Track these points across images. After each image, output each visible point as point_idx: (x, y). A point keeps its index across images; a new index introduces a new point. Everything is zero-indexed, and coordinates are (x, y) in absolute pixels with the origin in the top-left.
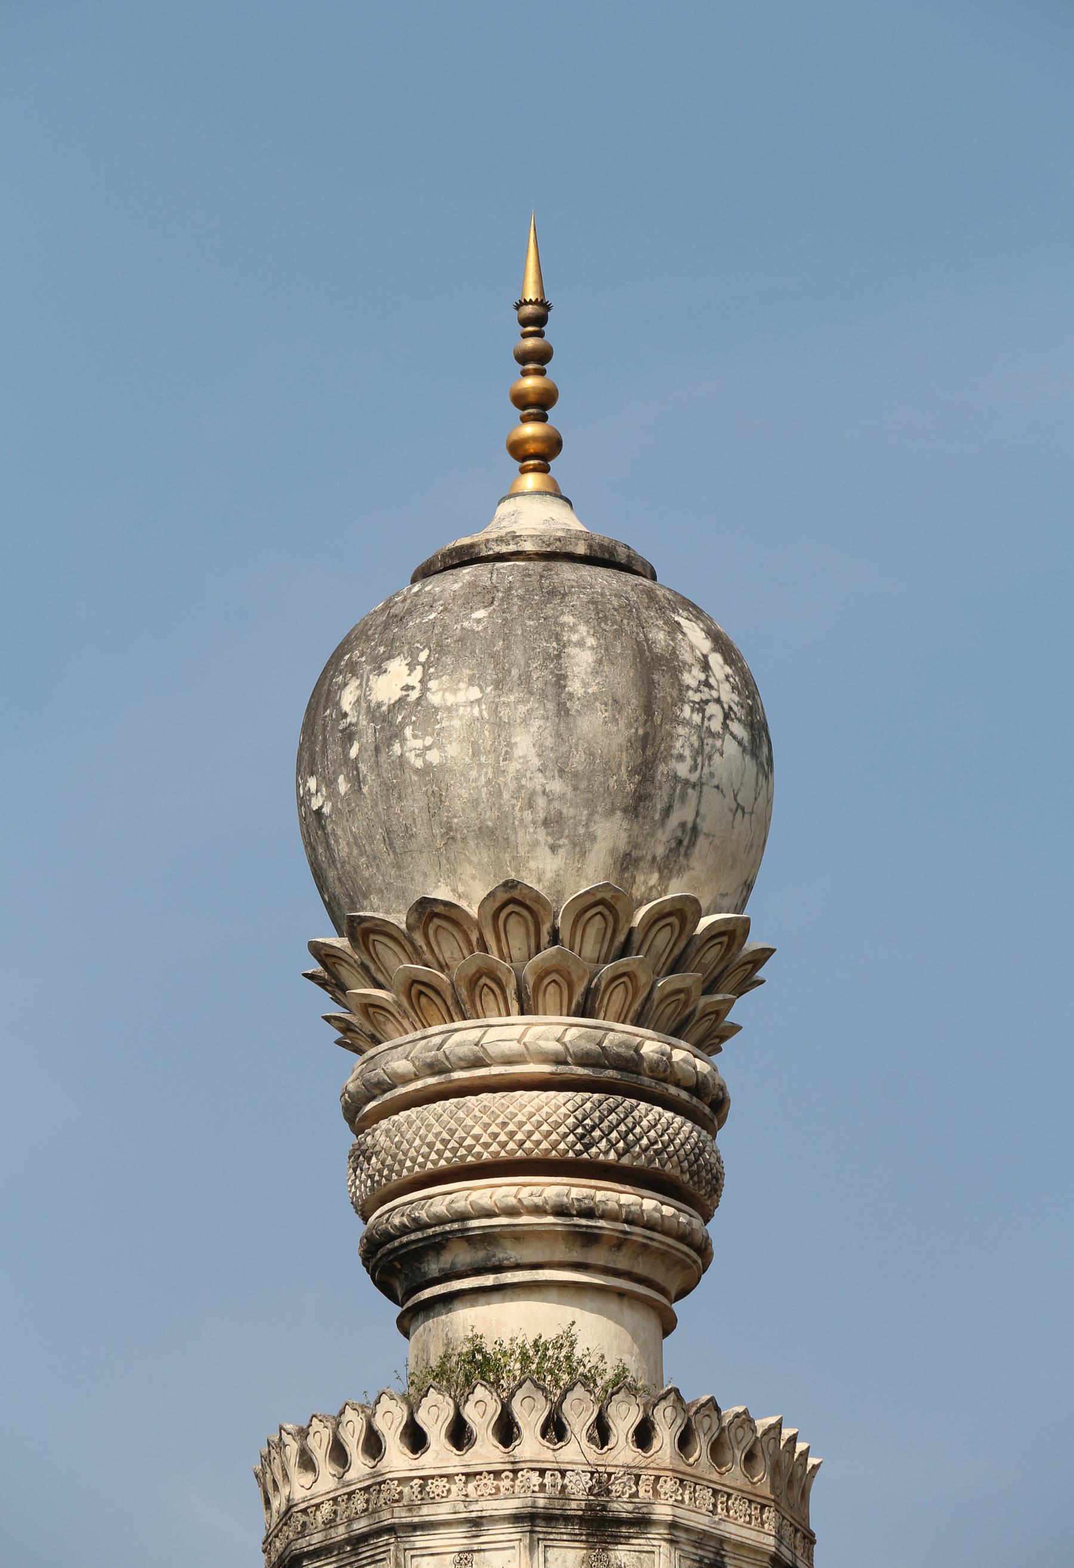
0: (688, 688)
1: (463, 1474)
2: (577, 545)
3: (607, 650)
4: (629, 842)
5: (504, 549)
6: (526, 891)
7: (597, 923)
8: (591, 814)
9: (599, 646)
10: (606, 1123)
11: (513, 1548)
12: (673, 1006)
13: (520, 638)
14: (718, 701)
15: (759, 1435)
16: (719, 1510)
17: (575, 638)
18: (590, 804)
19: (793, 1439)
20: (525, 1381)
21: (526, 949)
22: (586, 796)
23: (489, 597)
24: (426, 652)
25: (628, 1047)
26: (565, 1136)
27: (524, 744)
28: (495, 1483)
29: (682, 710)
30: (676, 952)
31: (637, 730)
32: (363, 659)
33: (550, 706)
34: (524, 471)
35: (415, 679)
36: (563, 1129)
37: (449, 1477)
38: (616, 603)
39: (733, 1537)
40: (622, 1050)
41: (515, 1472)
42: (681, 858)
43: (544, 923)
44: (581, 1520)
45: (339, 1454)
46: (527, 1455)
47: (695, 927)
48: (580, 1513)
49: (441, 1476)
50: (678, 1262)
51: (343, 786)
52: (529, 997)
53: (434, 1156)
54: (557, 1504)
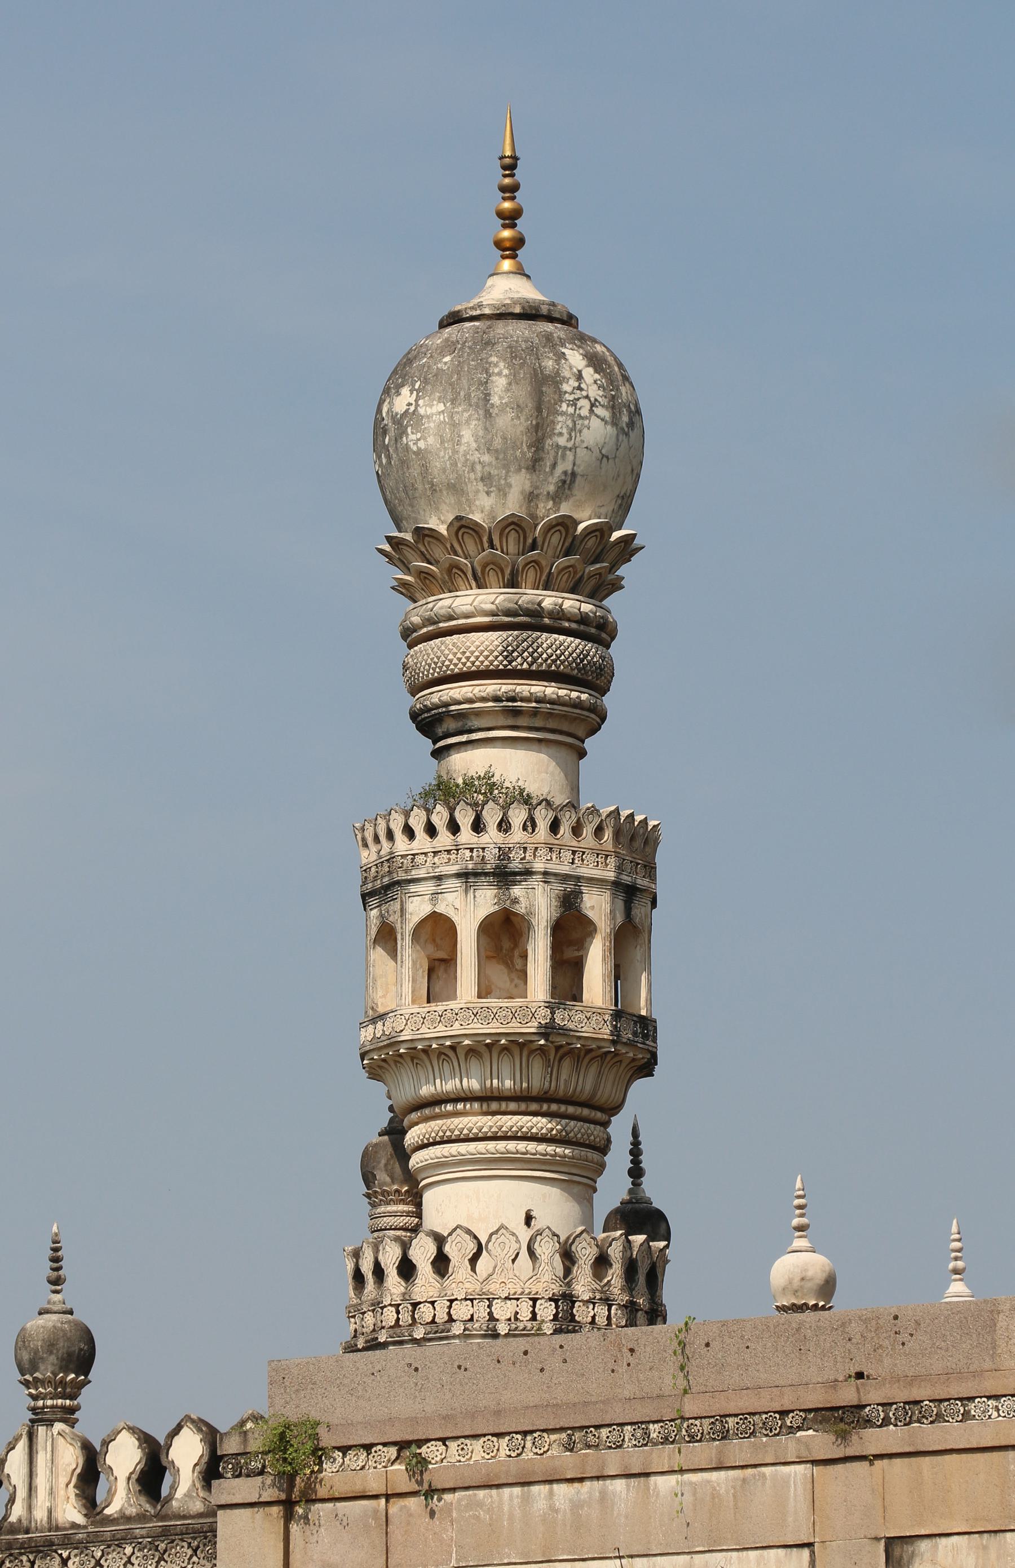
0: (566, 392)
1: (432, 852)
2: (515, 307)
3: (514, 376)
4: (531, 486)
5: (475, 313)
6: (469, 521)
7: (513, 535)
8: (508, 472)
9: (510, 374)
10: (521, 648)
11: (457, 891)
12: (566, 575)
13: (467, 373)
14: (587, 397)
15: (603, 818)
16: (576, 861)
17: (496, 370)
18: (506, 467)
19: (631, 816)
20: (460, 801)
21: (476, 551)
22: (503, 462)
23: (453, 348)
24: (419, 382)
25: (533, 604)
26: (497, 657)
27: (467, 435)
28: (448, 856)
29: (561, 407)
30: (567, 544)
31: (532, 421)
32: (392, 386)
33: (481, 412)
34: (504, 257)
35: (412, 400)
36: (496, 653)
37: (425, 854)
38: (524, 346)
39: (585, 875)
40: (530, 606)
41: (457, 850)
42: (566, 491)
43: (483, 537)
44: (494, 874)
45: (377, 839)
46: (463, 841)
47: (576, 529)
48: (492, 870)
49: (422, 854)
50: (575, 719)
51: (384, 461)
52: (480, 578)
53: (431, 671)
54: (479, 867)
